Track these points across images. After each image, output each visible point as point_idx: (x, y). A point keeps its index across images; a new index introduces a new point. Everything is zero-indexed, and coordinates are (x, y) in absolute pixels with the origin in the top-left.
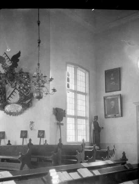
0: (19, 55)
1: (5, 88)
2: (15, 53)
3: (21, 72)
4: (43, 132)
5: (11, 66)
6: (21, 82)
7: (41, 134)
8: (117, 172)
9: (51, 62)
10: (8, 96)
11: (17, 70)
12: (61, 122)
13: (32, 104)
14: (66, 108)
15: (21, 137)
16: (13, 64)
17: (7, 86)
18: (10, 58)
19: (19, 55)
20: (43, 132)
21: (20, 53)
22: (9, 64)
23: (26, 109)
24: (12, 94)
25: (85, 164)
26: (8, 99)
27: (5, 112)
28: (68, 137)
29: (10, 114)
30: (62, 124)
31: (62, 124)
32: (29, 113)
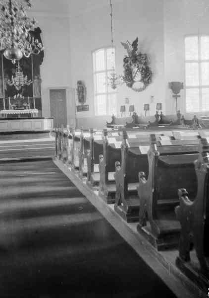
0: (137, 40)
1: (130, 69)
2: (134, 39)
3: (140, 55)
4: (161, 104)
5: (133, 51)
6: (140, 63)
7: (159, 106)
8: (166, 204)
9: (165, 45)
10: (134, 75)
11: (137, 53)
12: (178, 95)
13: (151, 80)
14: (185, 81)
15: (145, 109)
16: (134, 49)
17: (132, 67)
18: (132, 43)
19: (137, 40)
20: (161, 104)
21: (137, 39)
22: (131, 48)
23: (147, 86)
24: (136, 73)
25: (188, 136)
26: (134, 78)
27: (134, 89)
28: (52, 140)
29: (136, 90)
30: (179, 96)
31: (179, 96)
32: (151, 87)
